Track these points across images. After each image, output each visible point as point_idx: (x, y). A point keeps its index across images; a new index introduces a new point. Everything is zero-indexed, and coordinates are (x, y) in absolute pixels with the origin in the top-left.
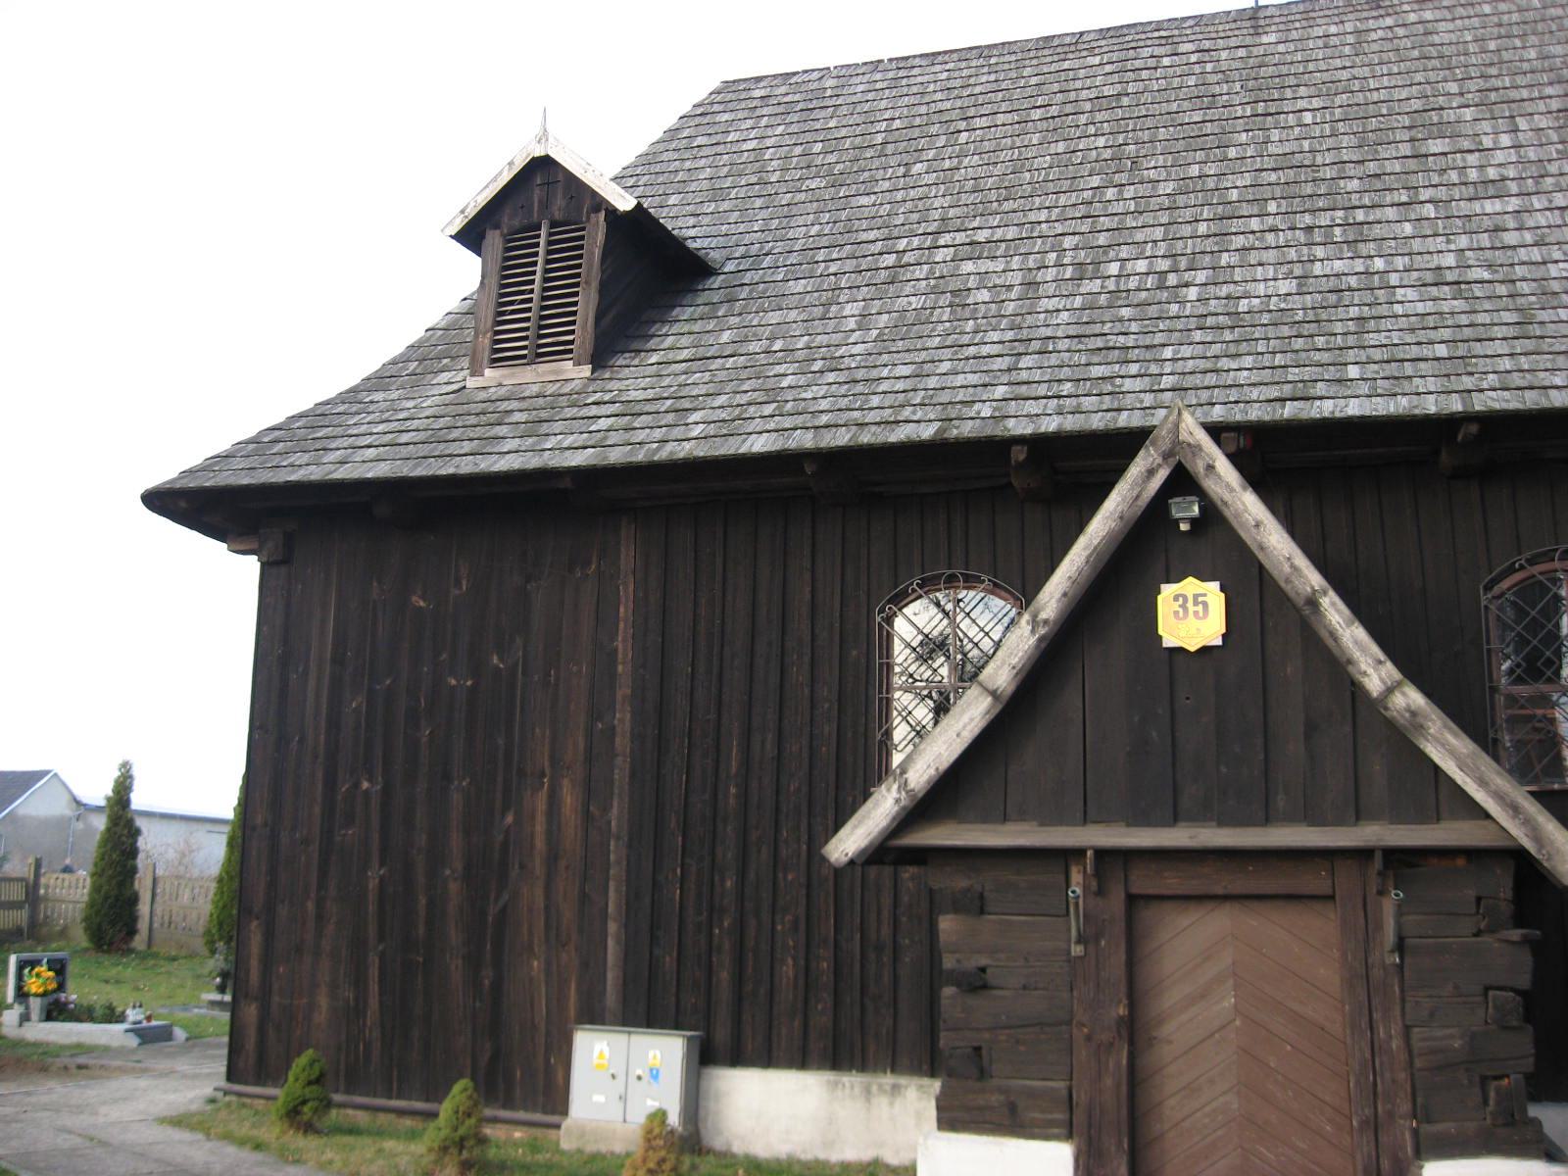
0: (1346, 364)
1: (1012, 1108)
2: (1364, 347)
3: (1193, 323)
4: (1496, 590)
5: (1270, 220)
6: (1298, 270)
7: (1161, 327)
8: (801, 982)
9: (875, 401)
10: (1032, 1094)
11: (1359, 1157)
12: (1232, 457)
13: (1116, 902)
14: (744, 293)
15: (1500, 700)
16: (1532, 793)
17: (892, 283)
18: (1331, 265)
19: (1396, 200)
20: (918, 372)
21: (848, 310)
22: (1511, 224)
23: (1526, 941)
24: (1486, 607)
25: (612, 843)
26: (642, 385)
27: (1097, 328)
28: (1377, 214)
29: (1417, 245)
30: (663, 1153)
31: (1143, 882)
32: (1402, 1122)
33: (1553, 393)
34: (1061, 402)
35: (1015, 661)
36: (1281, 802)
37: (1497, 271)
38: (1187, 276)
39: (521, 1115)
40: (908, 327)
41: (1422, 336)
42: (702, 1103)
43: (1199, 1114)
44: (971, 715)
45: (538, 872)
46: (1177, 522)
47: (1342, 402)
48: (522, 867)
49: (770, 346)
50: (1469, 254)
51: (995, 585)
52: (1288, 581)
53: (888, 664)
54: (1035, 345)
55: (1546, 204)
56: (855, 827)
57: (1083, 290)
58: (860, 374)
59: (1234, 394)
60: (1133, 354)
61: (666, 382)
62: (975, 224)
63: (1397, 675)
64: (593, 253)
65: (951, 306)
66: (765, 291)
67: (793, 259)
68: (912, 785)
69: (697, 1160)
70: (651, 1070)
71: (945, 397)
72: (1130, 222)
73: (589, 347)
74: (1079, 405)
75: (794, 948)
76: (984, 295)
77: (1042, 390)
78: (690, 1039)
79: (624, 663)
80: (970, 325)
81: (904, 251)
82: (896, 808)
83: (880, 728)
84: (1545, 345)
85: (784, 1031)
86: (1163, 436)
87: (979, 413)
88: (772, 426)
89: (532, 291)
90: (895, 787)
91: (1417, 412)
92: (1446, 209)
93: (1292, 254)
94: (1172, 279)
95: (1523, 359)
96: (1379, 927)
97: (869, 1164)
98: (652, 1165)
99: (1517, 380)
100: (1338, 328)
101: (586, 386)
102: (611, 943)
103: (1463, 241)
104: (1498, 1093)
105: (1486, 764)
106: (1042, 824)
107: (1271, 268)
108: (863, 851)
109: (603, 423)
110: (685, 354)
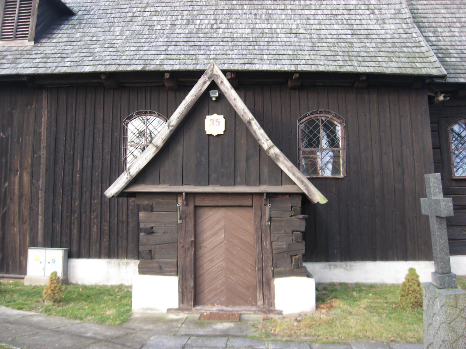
0: (263, 55)
1: (161, 267)
2: (269, 50)
3: (220, 40)
4: (301, 121)
5: (244, 11)
6: (252, 26)
7: (211, 40)
8: (99, 233)
9: (124, 57)
10: (166, 263)
11: (257, 278)
12: (230, 80)
13: (191, 207)
14: (84, 22)
15: (301, 152)
16: (308, 178)
17: (131, 21)
18: (261, 25)
19: (281, 8)
20: (138, 49)
21: (117, 29)
22: (312, 18)
23: (304, 218)
24: (298, 126)
25: (40, 192)
26: (51, 49)
27: (192, 39)
28: (275, 12)
29: (285, 21)
30: (56, 285)
31: (199, 202)
32: (269, 268)
33: (320, 66)
34: (180, 60)
35: (163, 137)
36: (238, 179)
37: (307, 31)
38: (220, 26)
39: (12, 275)
40: (136, 35)
41: (285, 48)
42: (69, 270)
43: (214, 267)
44: (150, 153)
45: (16, 201)
46: (212, 98)
47: (261, 65)
48: (11, 199)
49: (92, 39)
50: (300, 25)
51: (159, 115)
52: (243, 116)
53: (126, 138)
54: (173, 43)
55: (322, 13)
56: (114, 186)
57: (188, 28)
58: (120, 49)
59: (231, 61)
60: (202, 48)
61: (58, 48)
62: (157, 5)
63: (272, 144)
64: (35, 6)
65: (149, 30)
66: (91, 21)
67: (100, 12)
68: (131, 173)
69: (67, 286)
70: (53, 260)
71: (145, 57)
72: (204, 8)
73: (33, 36)
74: (185, 62)
75: (97, 223)
76: (159, 27)
77: (175, 57)
78: (65, 250)
79: (43, 136)
80: (154, 36)
81: (135, 12)
82: (127, 180)
83: (123, 157)
84: (318, 53)
85: (94, 248)
86: (209, 72)
87: (155, 63)
88: (91, 63)
89: (15, 17)
90: (127, 174)
91: (282, 69)
92: (294, 12)
93: (250, 21)
94: (215, 26)
95: (312, 56)
96: (265, 214)
97: (119, 286)
98: (52, 288)
99: (310, 62)
100: (262, 44)
101: (32, 48)
102: (40, 222)
103: (298, 22)
104: (295, 259)
105: (295, 169)
106: (170, 185)
107: (244, 25)
108: (116, 193)
109: (37, 60)
110: (65, 40)
